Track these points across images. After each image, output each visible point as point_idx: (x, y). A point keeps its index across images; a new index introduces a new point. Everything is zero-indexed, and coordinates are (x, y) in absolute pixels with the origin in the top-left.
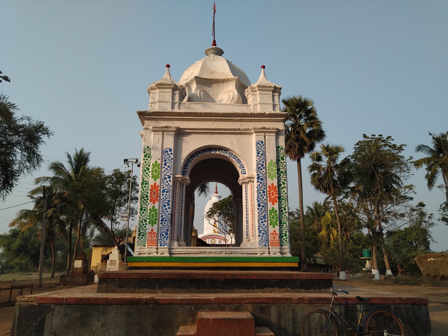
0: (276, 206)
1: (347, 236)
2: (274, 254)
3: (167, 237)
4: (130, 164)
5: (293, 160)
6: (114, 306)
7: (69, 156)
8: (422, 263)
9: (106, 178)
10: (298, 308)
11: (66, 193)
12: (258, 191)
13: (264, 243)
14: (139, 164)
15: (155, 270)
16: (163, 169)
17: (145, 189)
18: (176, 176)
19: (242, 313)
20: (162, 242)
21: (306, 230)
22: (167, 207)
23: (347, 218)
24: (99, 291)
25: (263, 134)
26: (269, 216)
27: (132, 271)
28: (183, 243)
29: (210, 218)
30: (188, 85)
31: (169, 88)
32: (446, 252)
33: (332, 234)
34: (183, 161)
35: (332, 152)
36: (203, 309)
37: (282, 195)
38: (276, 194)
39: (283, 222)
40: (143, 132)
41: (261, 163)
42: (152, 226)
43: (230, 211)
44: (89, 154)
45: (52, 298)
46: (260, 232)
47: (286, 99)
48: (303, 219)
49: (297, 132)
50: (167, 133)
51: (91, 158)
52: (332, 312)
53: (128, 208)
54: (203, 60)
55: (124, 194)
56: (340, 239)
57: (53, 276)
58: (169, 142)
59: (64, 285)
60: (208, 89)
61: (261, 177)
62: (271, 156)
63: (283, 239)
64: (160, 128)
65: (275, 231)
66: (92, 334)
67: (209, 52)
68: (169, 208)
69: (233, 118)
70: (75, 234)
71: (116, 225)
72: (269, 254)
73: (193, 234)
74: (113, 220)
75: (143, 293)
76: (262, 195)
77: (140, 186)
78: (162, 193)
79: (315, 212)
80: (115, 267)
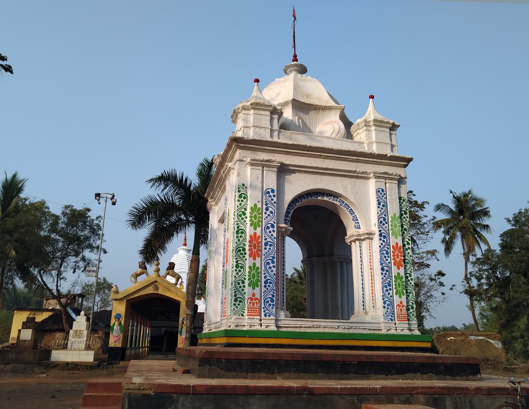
0: (402, 271)
2: (402, 330)
3: (273, 305)
6: (257, 396)
8: (441, 342)
12: (381, 251)
13: (390, 317)
14: (114, 201)
16: (264, 216)
17: (241, 239)
18: (281, 225)
20: (267, 312)
22: (271, 265)
25: (384, 180)
31: (266, 110)
32: (435, 329)
34: (286, 207)
37: (407, 258)
38: (401, 256)
39: (409, 291)
41: (383, 216)
42: (254, 289)
46: (385, 303)
58: (271, 180)
60: (304, 116)
61: (383, 234)
63: (409, 312)
64: (261, 161)
65: (401, 302)
68: (274, 267)
69: (348, 157)
72: (396, 330)
76: (385, 257)
78: (264, 247)
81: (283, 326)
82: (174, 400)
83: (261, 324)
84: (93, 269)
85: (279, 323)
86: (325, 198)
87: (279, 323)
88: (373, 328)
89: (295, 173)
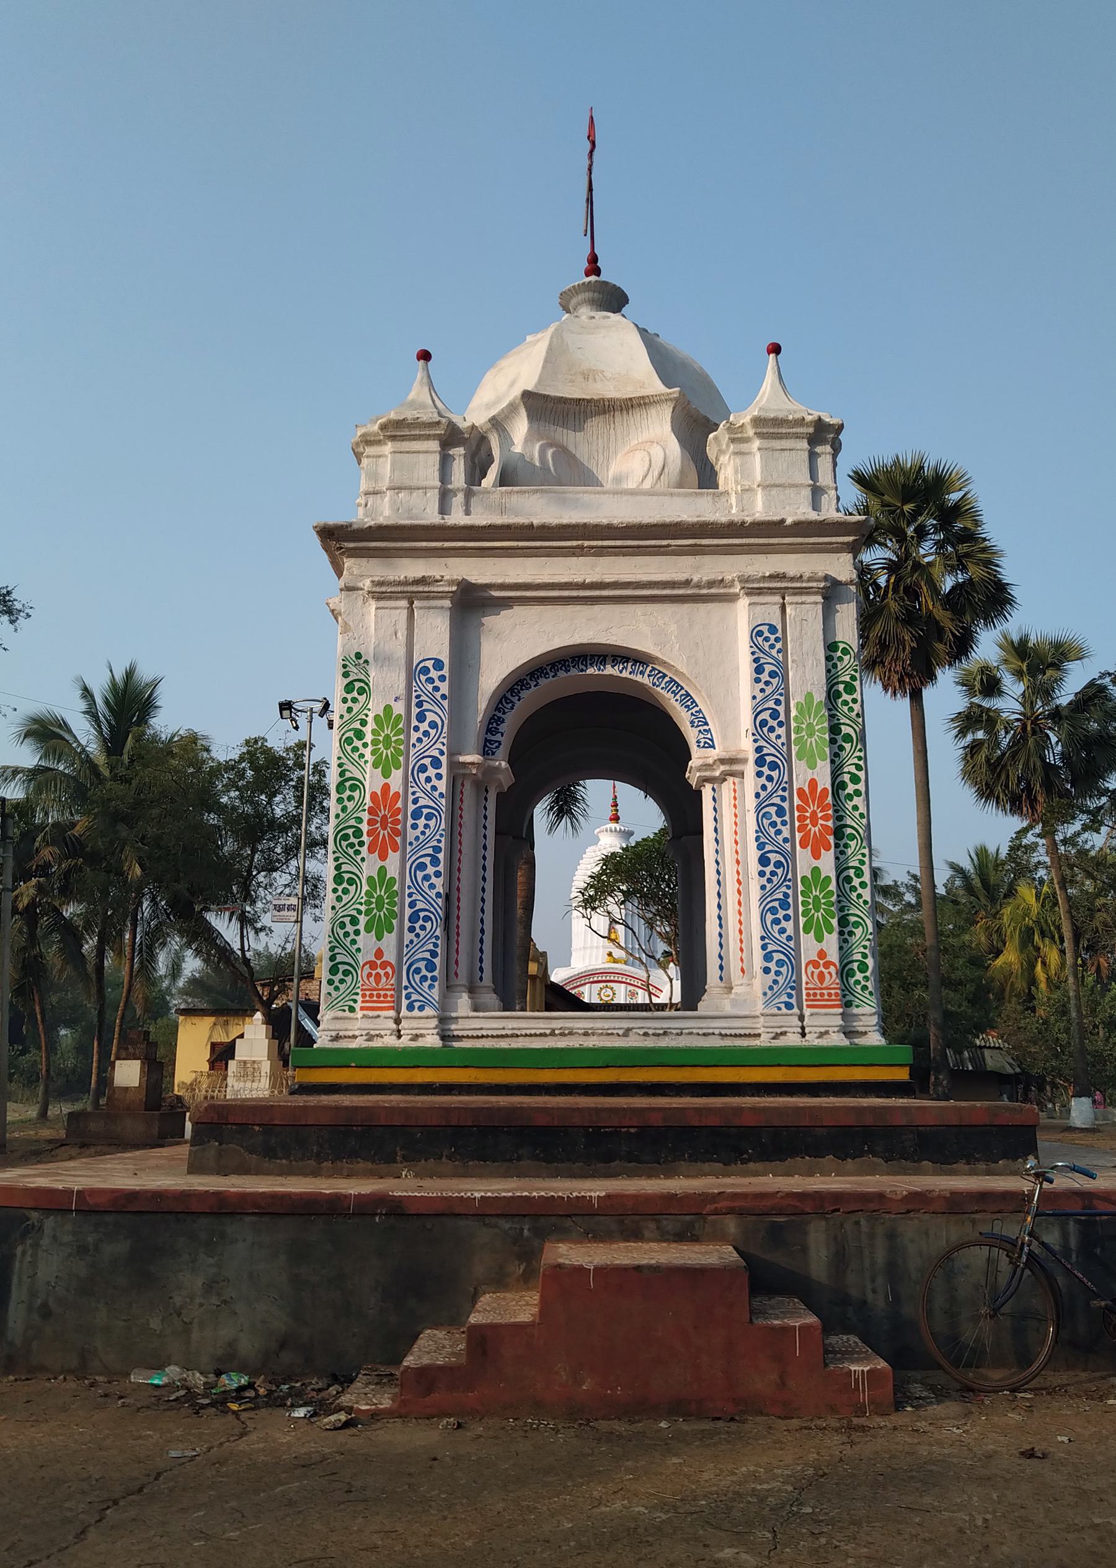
0: (827, 863)
1: (1098, 970)
2: (821, 1035)
3: (434, 979)
4: (302, 719)
5: (894, 693)
6: (248, 1219)
7: (87, 693)
9: (219, 769)
10: (909, 1229)
11: (82, 823)
13: (784, 998)
15: (392, 1097)
16: (414, 736)
17: (350, 805)
18: (462, 759)
19: (703, 1248)
20: (414, 997)
21: (946, 950)
22: (431, 870)
23: (1100, 902)
24: (195, 1168)
25: (777, 599)
26: (800, 898)
27: (311, 1098)
28: (491, 998)
29: (594, 909)
30: (498, 423)
31: (428, 437)
33: (1044, 963)
34: (483, 705)
35: (1039, 661)
36: (563, 1234)
37: (849, 822)
38: (826, 818)
39: (853, 919)
40: (338, 600)
43: (663, 882)
44: (155, 684)
45: (32, 1189)
46: (768, 957)
47: (867, 469)
48: (935, 910)
49: (907, 590)
50: (425, 603)
51: (164, 697)
52: (1035, 1242)
53: (298, 876)
54: (551, 329)
55: (284, 829)
56: (1071, 980)
57: (43, 1114)
58: (434, 634)
59: (83, 1146)
60: (569, 438)
61: (769, 759)
62: (807, 678)
64: (400, 583)
65: (822, 954)
66: (175, 1316)
67: (574, 301)
68: (438, 874)
69: (665, 542)
70: (118, 970)
71: (258, 940)
72: (803, 1035)
73: (533, 968)
74: (246, 921)
75: (349, 1176)
77: (334, 795)
78: (410, 822)
79: (977, 882)
80: (255, 1085)
81: (465, 1033)
82: (33, 1226)
83: (399, 1031)
84: (288, 903)
85: (453, 1027)
86: (609, 670)
87: (453, 1027)
88: (733, 1032)
89: (511, 607)
